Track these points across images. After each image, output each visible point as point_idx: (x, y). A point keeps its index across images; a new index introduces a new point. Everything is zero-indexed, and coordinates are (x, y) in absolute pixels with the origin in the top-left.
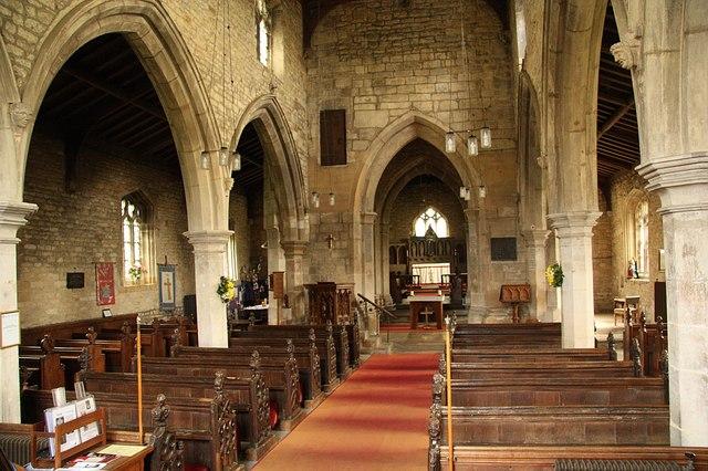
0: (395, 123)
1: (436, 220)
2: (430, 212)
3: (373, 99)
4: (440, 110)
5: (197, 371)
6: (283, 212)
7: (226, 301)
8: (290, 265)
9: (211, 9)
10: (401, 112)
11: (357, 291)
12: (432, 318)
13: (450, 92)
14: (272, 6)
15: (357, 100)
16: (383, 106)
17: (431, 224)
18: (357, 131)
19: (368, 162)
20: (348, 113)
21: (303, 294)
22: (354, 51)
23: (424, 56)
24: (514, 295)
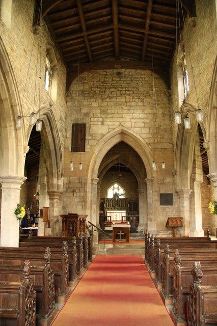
0: (112, 132)
1: (119, 189)
2: (116, 185)
4: (135, 127)
6: (49, 175)
7: (20, 219)
8: (52, 204)
9: (24, 50)
10: (114, 127)
11: (88, 219)
12: (123, 237)
13: (140, 118)
14: (53, 65)
15: (92, 119)
16: (106, 123)
17: (116, 190)
18: (92, 135)
19: (96, 152)
20: (87, 125)
21: (58, 221)
22: (91, 95)
23: (128, 100)
24: (175, 223)
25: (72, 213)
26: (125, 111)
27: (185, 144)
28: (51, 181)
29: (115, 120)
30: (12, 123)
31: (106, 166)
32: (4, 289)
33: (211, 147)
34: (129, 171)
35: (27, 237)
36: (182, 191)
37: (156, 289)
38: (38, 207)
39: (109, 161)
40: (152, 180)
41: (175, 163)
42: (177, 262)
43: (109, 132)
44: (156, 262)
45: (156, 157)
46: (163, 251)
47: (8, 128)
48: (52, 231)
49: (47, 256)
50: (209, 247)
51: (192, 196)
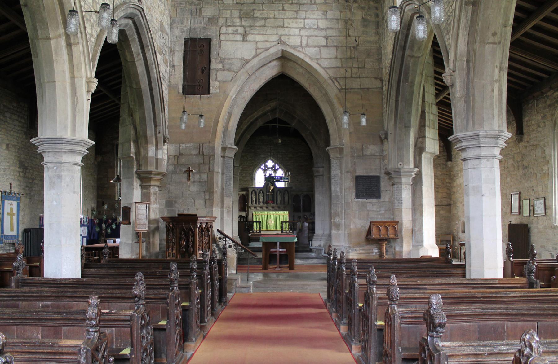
3: (241, 30)
4: (308, 46)
5: (48, 306)
10: (268, 45)
11: (216, 226)
15: (224, 30)
16: (250, 37)
18: (222, 61)
19: (232, 94)
20: (214, 42)
21: (157, 229)
24: (383, 231)
25: (186, 213)
26: (290, 14)
27: (406, 79)
28: (143, 152)
29: (270, 31)
30: (61, 30)
31: (252, 124)
32: (49, 353)
33: (458, 80)
34: (296, 134)
35: (99, 260)
36: (398, 171)
37: (349, 354)
38: (119, 202)
39: (256, 114)
40: (341, 150)
41: (385, 117)
42: (392, 300)
43: (257, 55)
44: (350, 303)
45: (348, 105)
46: (363, 281)
47: (53, 42)
48: (148, 249)
49: (139, 290)
50: (450, 275)
51: (417, 181)
